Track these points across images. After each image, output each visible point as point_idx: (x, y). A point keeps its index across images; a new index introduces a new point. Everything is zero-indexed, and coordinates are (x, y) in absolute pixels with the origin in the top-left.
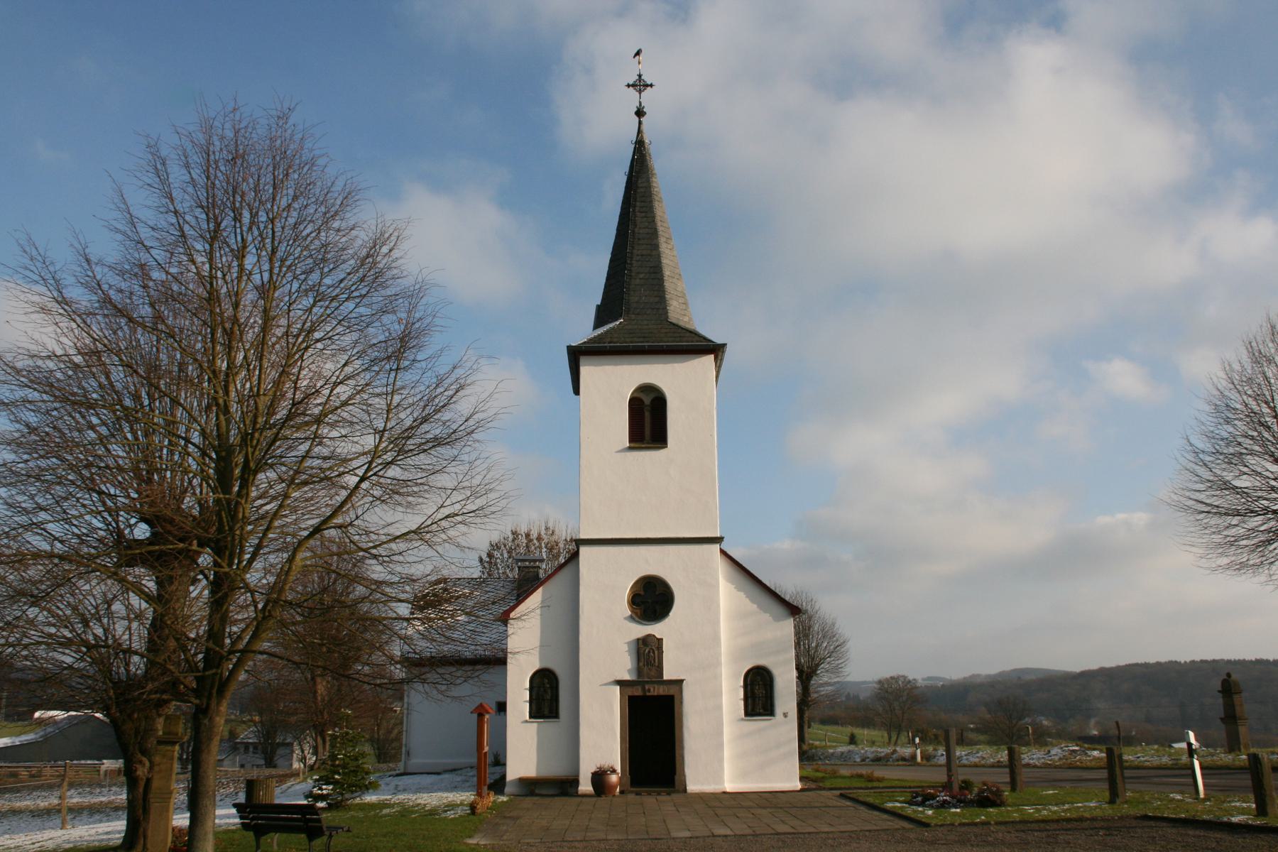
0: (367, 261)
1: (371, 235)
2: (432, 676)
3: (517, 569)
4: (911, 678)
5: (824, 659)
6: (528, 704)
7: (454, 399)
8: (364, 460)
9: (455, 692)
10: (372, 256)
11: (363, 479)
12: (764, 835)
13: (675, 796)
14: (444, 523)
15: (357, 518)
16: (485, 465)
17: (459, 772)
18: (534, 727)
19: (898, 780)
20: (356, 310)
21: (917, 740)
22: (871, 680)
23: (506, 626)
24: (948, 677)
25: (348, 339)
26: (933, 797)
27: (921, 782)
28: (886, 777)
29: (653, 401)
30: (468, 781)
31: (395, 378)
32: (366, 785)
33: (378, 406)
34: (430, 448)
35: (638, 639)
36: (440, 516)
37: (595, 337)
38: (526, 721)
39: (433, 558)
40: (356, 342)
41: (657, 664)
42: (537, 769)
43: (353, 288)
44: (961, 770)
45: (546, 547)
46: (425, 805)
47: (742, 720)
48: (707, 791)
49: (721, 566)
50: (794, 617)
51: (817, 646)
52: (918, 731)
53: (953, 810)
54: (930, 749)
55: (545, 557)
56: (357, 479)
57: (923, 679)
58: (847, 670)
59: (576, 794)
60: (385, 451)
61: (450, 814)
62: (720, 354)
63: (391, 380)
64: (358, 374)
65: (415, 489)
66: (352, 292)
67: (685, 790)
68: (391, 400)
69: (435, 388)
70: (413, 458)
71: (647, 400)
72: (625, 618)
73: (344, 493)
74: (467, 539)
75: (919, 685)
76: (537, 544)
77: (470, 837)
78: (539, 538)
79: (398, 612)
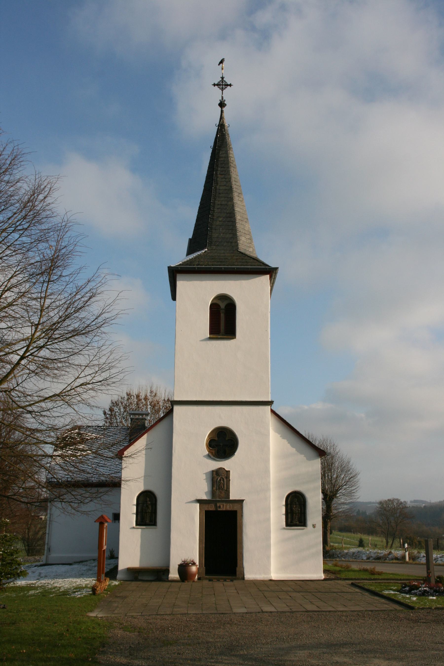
0: (28, 205)
1: (31, 186)
2: (68, 497)
3: (130, 420)
4: (402, 500)
5: (342, 486)
6: (135, 516)
7: (88, 303)
8: (23, 344)
9: (84, 508)
10: (32, 201)
11: (22, 358)
12: (298, 612)
13: (236, 582)
14: (78, 389)
15: (18, 385)
16: (109, 350)
17: (85, 563)
18: (138, 532)
19: (392, 574)
20: (20, 239)
21: (406, 546)
22: (374, 501)
23: (122, 461)
24: (429, 501)
25: (13, 260)
26: (417, 588)
27: (408, 576)
28: (384, 571)
29: (227, 306)
30: (91, 570)
31: (47, 287)
32: (18, 573)
33: (34, 307)
34: (71, 337)
35: (213, 471)
36: (77, 384)
37: (187, 261)
38: (134, 528)
39: (71, 414)
40: (20, 262)
41: (225, 489)
42: (140, 565)
43: (18, 224)
44: (436, 568)
45: (150, 405)
46: (60, 587)
47: (284, 529)
48: (259, 579)
49: (271, 421)
50: (321, 457)
51: (337, 477)
52: (407, 538)
53: (431, 598)
54: (415, 552)
55: (149, 412)
56: (19, 357)
57: (411, 502)
58: (358, 494)
59: (167, 580)
60: (39, 338)
61: (78, 595)
62: (274, 274)
63: (44, 289)
64: (21, 284)
65: (59, 365)
66: (17, 226)
67: (243, 578)
68: (44, 303)
69: (75, 295)
70: (58, 343)
71: (223, 305)
72: (204, 456)
73: (9, 367)
74: (95, 401)
75: (408, 506)
76: (144, 402)
77: (91, 611)
78: (146, 399)
79: (46, 451)
